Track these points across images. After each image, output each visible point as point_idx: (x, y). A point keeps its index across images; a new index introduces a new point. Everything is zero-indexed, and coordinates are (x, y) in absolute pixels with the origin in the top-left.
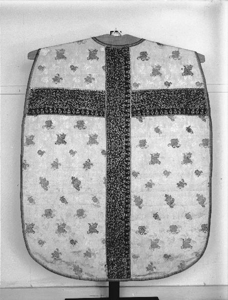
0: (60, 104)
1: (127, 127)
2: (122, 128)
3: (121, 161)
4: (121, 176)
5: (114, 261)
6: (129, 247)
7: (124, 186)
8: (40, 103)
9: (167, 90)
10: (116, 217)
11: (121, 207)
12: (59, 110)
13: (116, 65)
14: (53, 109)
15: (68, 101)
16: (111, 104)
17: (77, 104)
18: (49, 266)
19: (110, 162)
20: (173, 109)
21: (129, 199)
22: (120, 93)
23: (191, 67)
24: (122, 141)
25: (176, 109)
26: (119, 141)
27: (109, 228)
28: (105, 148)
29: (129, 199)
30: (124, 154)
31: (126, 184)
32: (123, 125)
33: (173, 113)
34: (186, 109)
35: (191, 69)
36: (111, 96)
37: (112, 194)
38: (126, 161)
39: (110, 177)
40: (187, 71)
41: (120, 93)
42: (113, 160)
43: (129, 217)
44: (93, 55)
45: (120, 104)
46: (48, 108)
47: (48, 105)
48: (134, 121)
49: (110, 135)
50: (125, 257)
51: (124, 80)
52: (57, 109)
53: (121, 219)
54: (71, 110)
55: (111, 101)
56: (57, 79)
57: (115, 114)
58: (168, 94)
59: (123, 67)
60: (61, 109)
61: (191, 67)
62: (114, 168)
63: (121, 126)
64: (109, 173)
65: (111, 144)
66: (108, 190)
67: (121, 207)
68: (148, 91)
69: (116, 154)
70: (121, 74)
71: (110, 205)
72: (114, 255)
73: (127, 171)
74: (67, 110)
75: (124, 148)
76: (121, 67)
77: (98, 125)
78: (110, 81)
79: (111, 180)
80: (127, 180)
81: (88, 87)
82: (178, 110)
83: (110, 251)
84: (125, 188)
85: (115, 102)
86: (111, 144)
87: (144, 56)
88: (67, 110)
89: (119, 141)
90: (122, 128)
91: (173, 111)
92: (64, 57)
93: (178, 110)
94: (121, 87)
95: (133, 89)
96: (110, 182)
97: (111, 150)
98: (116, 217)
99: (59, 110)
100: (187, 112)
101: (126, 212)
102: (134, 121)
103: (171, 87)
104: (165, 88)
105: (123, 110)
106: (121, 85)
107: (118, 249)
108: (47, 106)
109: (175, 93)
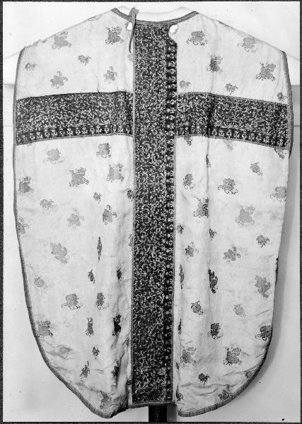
0: (68, 120)
1: (170, 153)
2: (160, 155)
3: (160, 208)
4: (159, 234)
5: (145, 373)
6: (170, 350)
7: (164, 249)
8: (42, 119)
9: (229, 99)
10: (150, 300)
11: (158, 283)
12: (69, 130)
13: (151, 53)
14: (57, 130)
15: (80, 114)
16: (143, 115)
17: (95, 116)
18: (49, 356)
19: (140, 210)
20: (233, 130)
21: (172, 270)
22: (158, 98)
23: (273, 66)
24: (160, 175)
25: (239, 130)
26: (156, 175)
27: (138, 319)
28: (132, 187)
29: (172, 270)
30: (163, 199)
31: (167, 247)
32: (163, 150)
33: (232, 137)
34: (256, 135)
35: (272, 71)
36: (142, 102)
37: (142, 263)
38: (167, 208)
39: (140, 235)
40: (266, 73)
41: (158, 98)
42: (145, 207)
43: (171, 300)
44: (113, 37)
45: (158, 115)
46: (49, 130)
47: (48, 124)
48: (180, 142)
49: (142, 165)
50: (163, 366)
51: (165, 77)
52: (65, 129)
53: (159, 303)
54: (88, 128)
55: (143, 110)
56: (57, 81)
57: (150, 131)
58: (230, 104)
59: (164, 181)
60: (71, 127)
61: (273, 66)
62: (147, 220)
63: (159, 152)
64: (138, 228)
65: (141, 181)
66: (137, 256)
67: (158, 283)
68: (202, 95)
69: (151, 197)
70: (160, 68)
71: (139, 280)
72: (145, 365)
73: (168, 224)
74: (81, 128)
75: (165, 187)
76: (160, 55)
77: (122, 147)
78: (143, 76)
79: (141, 239)
80: (168, 239)
81: (109, 87)
82: (241, 133)
83: (138, 357)
84: (165, 252)
85: (149, 111)
86: (141, 181)
87: (198, 36)
88: (81, 128)
89: (156, 175)
90: (160, 155)
91: (233, 133)
92: (66, 44)
93: (241, 133)
94: (160, 88)
95: (180, 91)
96: (139, 242)
97: (142, 191)
98: (150, 300)
99: (69, 130)
100: (253, 136)
101: (166, 293)
102: (180, 142)
103: (236, 94)
104: (227, 93)
105: (163, 125)
106: (160, 84)
107: (153, 353)
108: (46, 126)
109: (240, 105)
